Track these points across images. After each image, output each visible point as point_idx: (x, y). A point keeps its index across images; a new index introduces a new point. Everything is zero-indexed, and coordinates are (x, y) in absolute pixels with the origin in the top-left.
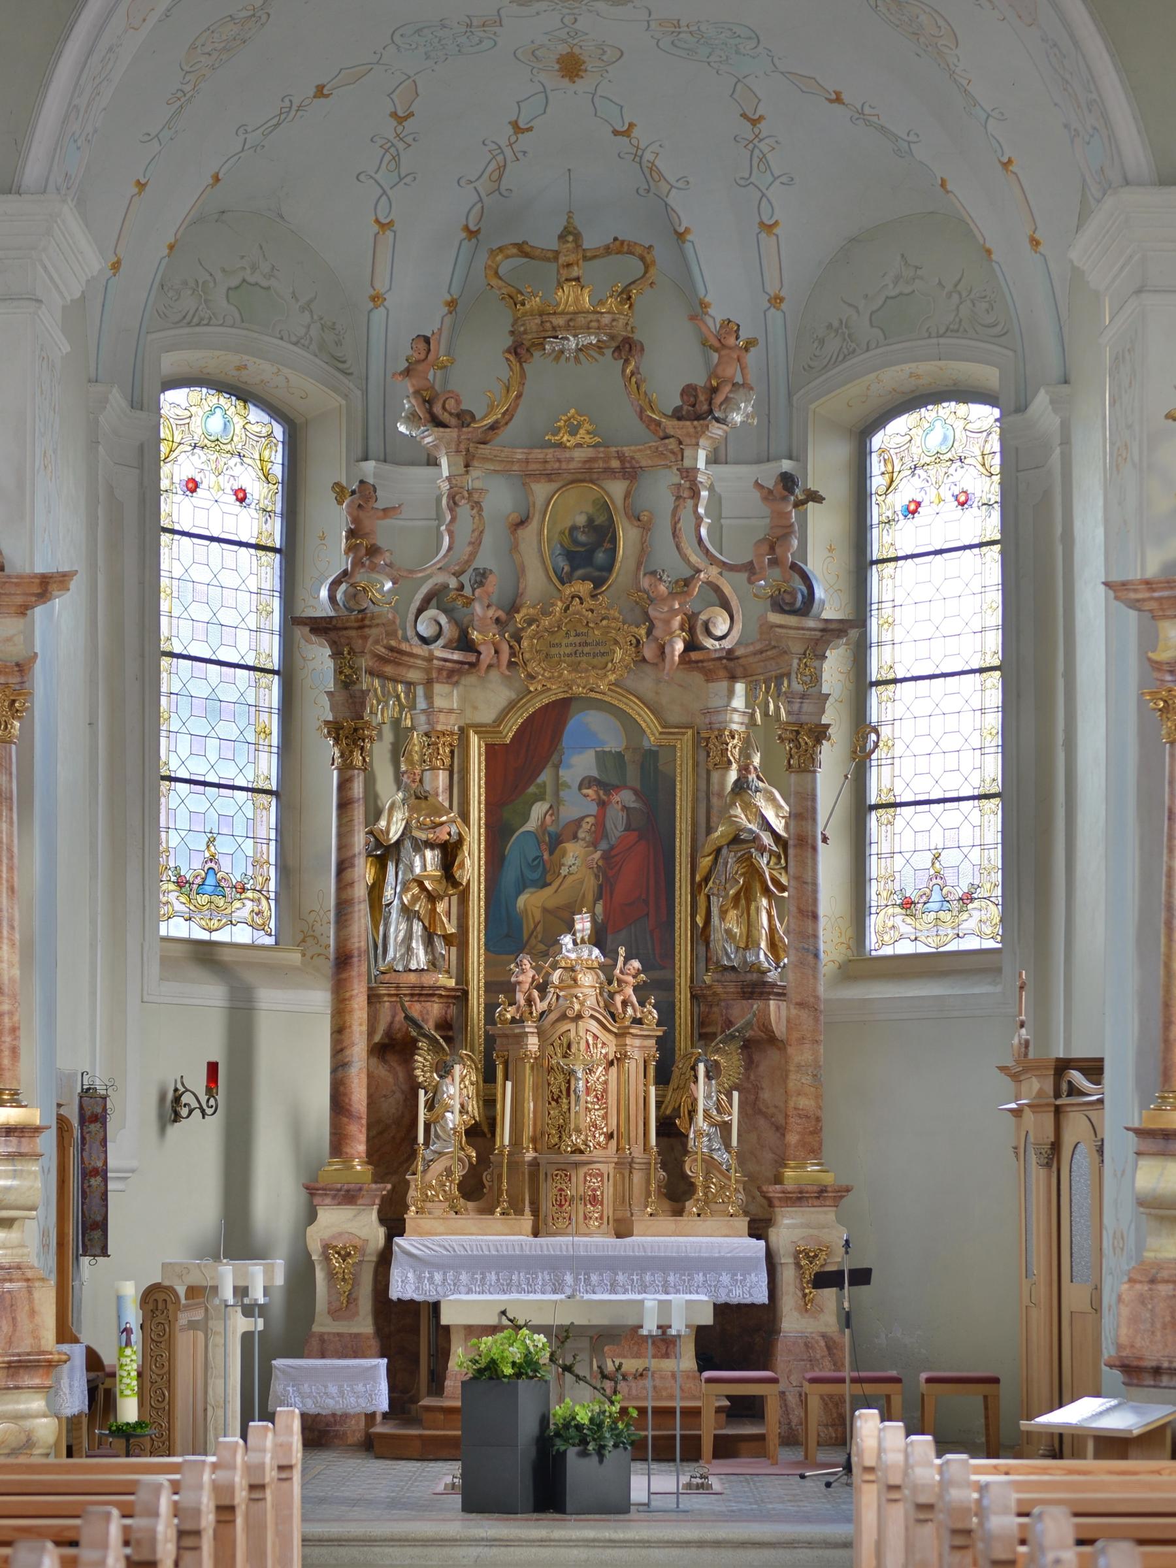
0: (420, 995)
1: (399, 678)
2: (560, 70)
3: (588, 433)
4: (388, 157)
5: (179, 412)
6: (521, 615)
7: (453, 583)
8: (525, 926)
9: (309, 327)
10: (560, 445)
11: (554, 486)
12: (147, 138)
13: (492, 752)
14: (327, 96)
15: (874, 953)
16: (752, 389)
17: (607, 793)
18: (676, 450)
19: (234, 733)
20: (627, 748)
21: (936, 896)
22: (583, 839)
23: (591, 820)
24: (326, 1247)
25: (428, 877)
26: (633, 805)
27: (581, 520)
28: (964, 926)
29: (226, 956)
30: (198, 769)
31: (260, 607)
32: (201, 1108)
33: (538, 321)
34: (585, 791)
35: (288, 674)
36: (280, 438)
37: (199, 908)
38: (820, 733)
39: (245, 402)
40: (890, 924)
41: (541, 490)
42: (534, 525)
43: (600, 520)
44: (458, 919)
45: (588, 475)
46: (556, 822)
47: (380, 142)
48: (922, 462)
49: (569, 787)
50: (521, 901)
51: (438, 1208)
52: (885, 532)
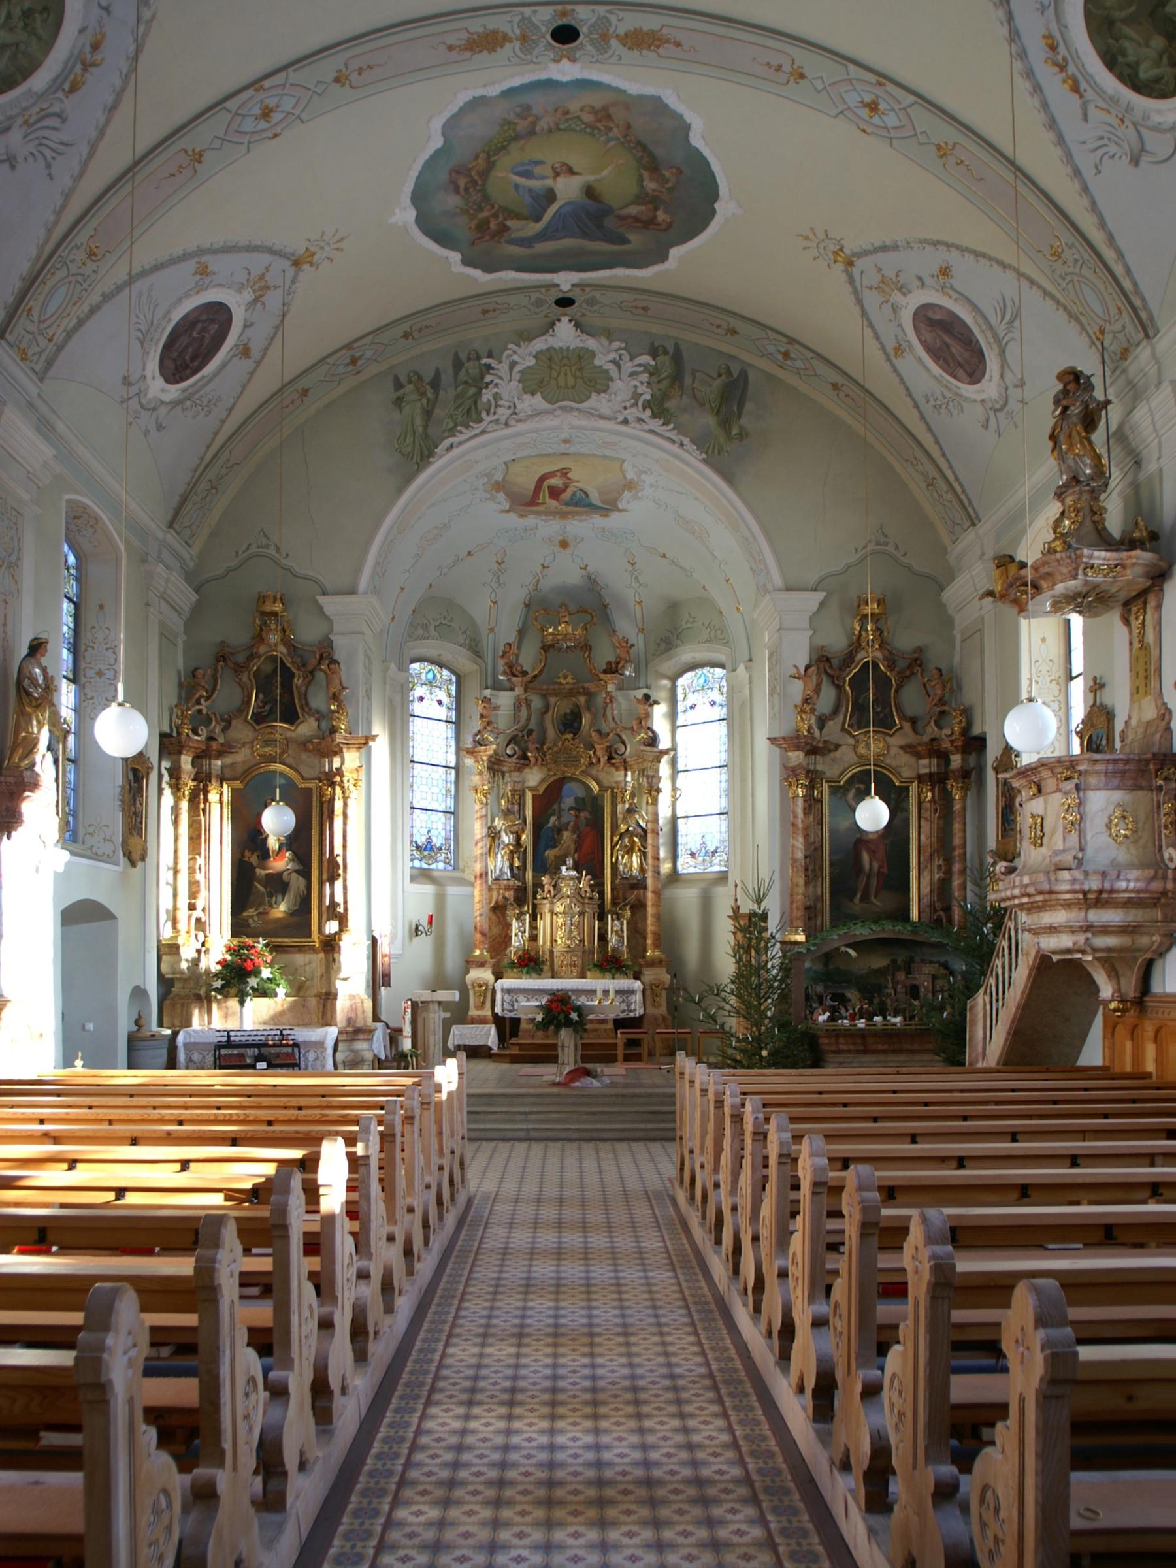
13: (534, 797)
29: (435, 874)
41: (552, 700)
45: (572, 693)
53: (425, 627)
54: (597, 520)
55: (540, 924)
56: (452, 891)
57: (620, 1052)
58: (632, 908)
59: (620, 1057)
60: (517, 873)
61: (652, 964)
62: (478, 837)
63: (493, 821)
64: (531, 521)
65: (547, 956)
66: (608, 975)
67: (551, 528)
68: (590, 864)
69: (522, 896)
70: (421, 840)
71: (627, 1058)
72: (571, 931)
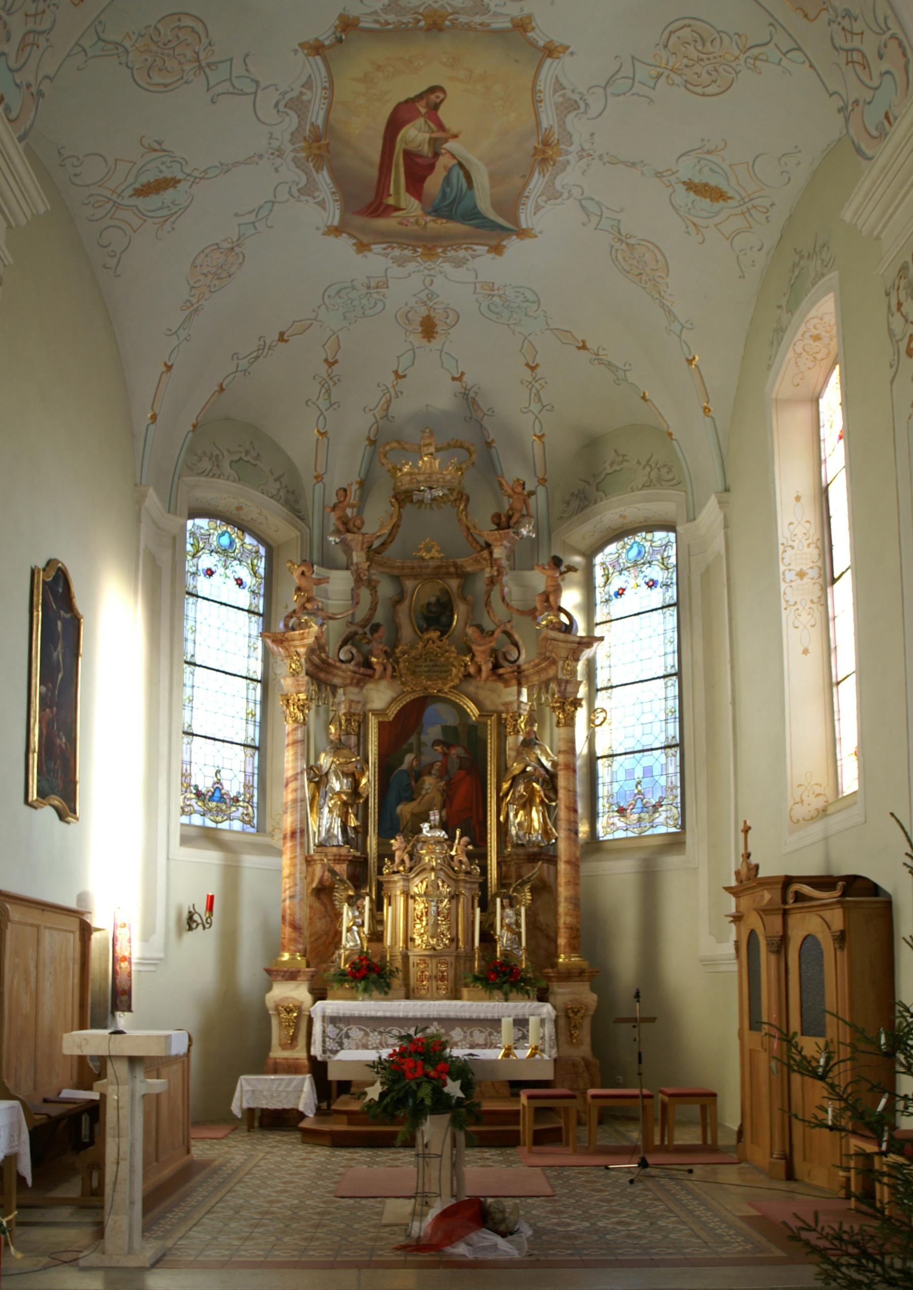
2: (423, 332)
4: (323, 390)
5: (202, 531)
7: (361, 631)
10: (422, 558)
11: (418, 581)
12: (169, 333)
13: (381, 725)
14: (286, 341)
21: (639, 805)
24: (276, 1009)
28: (657, 820)
29: (227, 837)
32: (203, 923)
34: (436, 748)
35: (266, 682)
37: (210, 810)
38: (576, 703)
39: (243, 532)
41: (409, 584)
42: (406, 603)
43: (444, 599)
45: (439, 573)
46: (419, 764)
47: (320, 380)
50: (399, 809)
53: (216, 460)
54: (483, 264)
55: (388, 912)
56: (250, 862)
58: (532, 890)
60: (354, 838)
61: (568, 976)
63: (317, 758)
64: (377, 261)
65: (398, 963)
66: (498, 994)
67: (406, 279)
68: (466, 819)
69: (359, 873)
70: (205, 783)
71: (541, 1138)
72: (436, 925)
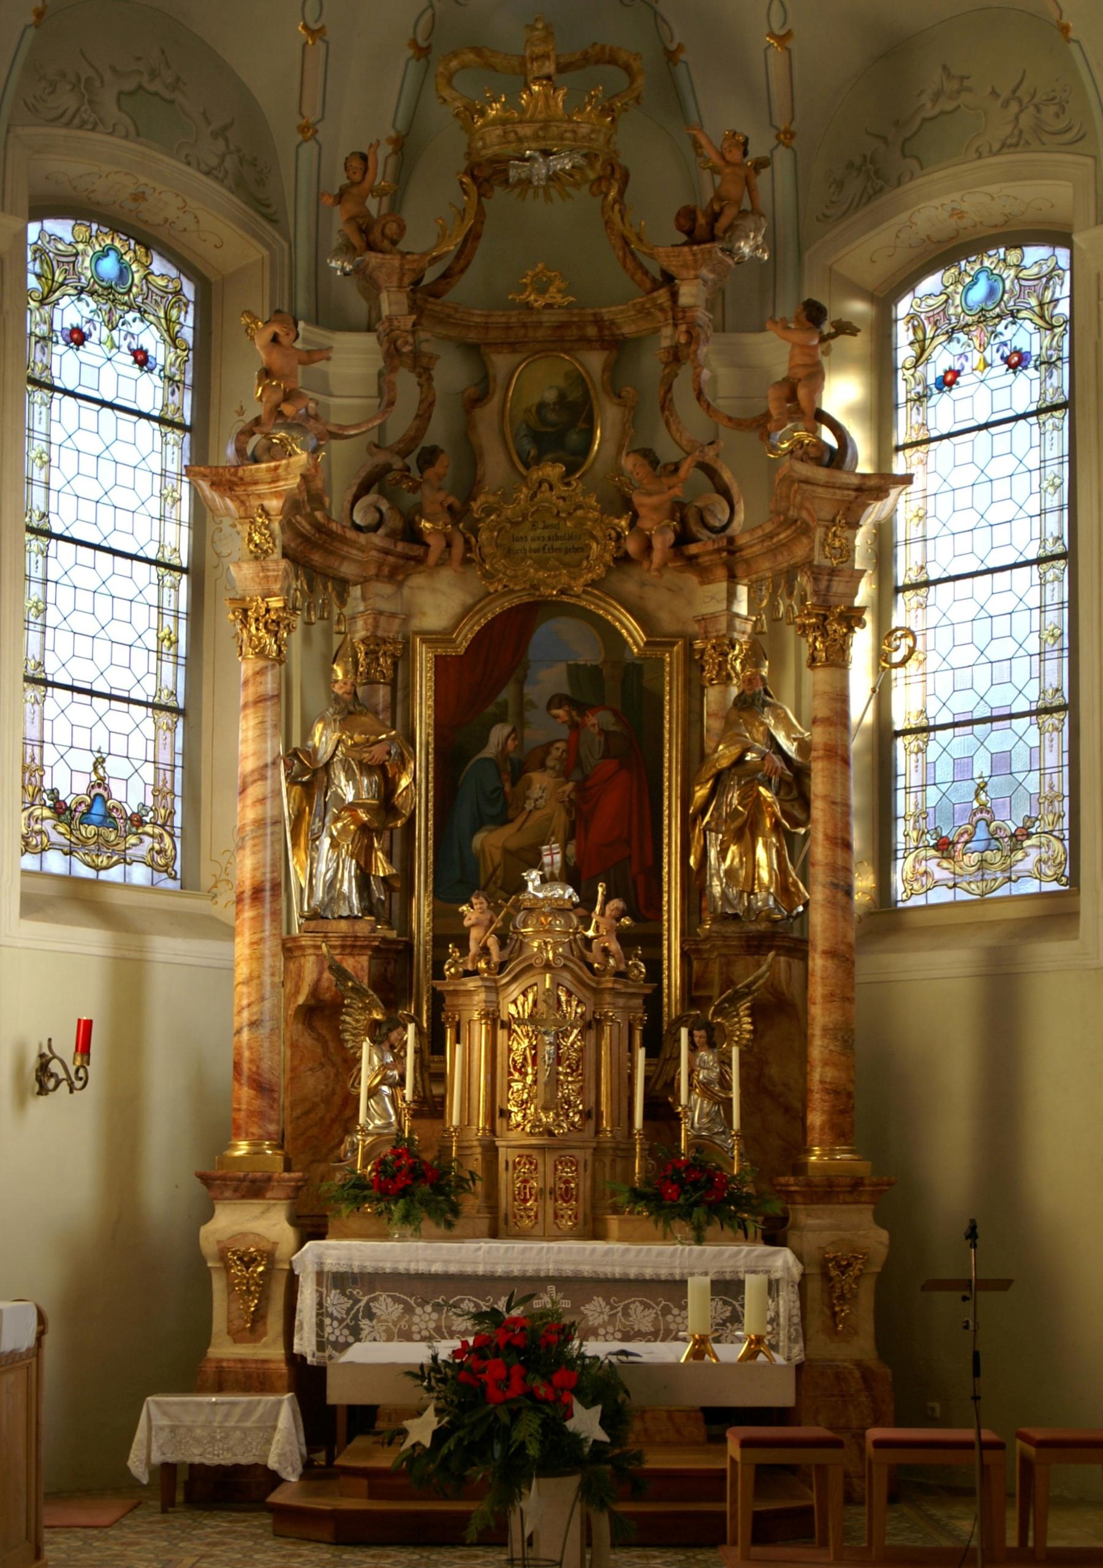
0: (354, 947)
1: (330, 573)
3: (559, 291)
6: (479, 502)
7: (398, 464)
8: (482, 869)
9: (223, 158)
10: (528, 307)
13: (441, 665)
15: (900, 905)
16: (763, 215)
17: (582, 714)
18: (667, 304)
19: (130, 637)
20: (605, 662)
22: (553, 768)
23: (561, 745)
25: (362, 806)
26: (612, 728)
27: (551, 396)
28: (1020, 866)
29: (118, 898)
30: (83, 675)
31: (165, 492)
33: (499, 131)
36: (192, 298)
37: (83, 842)
39: (148, 249)
40: (922, 869)
41: (501, 362)
42: (495, 402)
43: (574, 396)
44: (402, 861)
46: (520, 747)
48: (962, 323)
49: (535, 707)
50: (478, 840)
51: (345, 1209)
52: (915, 410)
55: (455, 1056)
56: (168, 950)
57: (739, 1506)
58: (753, 1012)
59: (740, 1526)
60: (385, 900)
61: (828, 1191)
62: (249, 765)
65: (475, 1163)
66: (680, 1227)
68: (619, 860)
70: (69, 781)
71: (766, 1530)
72: (554, 1082)
